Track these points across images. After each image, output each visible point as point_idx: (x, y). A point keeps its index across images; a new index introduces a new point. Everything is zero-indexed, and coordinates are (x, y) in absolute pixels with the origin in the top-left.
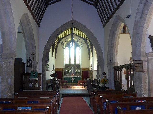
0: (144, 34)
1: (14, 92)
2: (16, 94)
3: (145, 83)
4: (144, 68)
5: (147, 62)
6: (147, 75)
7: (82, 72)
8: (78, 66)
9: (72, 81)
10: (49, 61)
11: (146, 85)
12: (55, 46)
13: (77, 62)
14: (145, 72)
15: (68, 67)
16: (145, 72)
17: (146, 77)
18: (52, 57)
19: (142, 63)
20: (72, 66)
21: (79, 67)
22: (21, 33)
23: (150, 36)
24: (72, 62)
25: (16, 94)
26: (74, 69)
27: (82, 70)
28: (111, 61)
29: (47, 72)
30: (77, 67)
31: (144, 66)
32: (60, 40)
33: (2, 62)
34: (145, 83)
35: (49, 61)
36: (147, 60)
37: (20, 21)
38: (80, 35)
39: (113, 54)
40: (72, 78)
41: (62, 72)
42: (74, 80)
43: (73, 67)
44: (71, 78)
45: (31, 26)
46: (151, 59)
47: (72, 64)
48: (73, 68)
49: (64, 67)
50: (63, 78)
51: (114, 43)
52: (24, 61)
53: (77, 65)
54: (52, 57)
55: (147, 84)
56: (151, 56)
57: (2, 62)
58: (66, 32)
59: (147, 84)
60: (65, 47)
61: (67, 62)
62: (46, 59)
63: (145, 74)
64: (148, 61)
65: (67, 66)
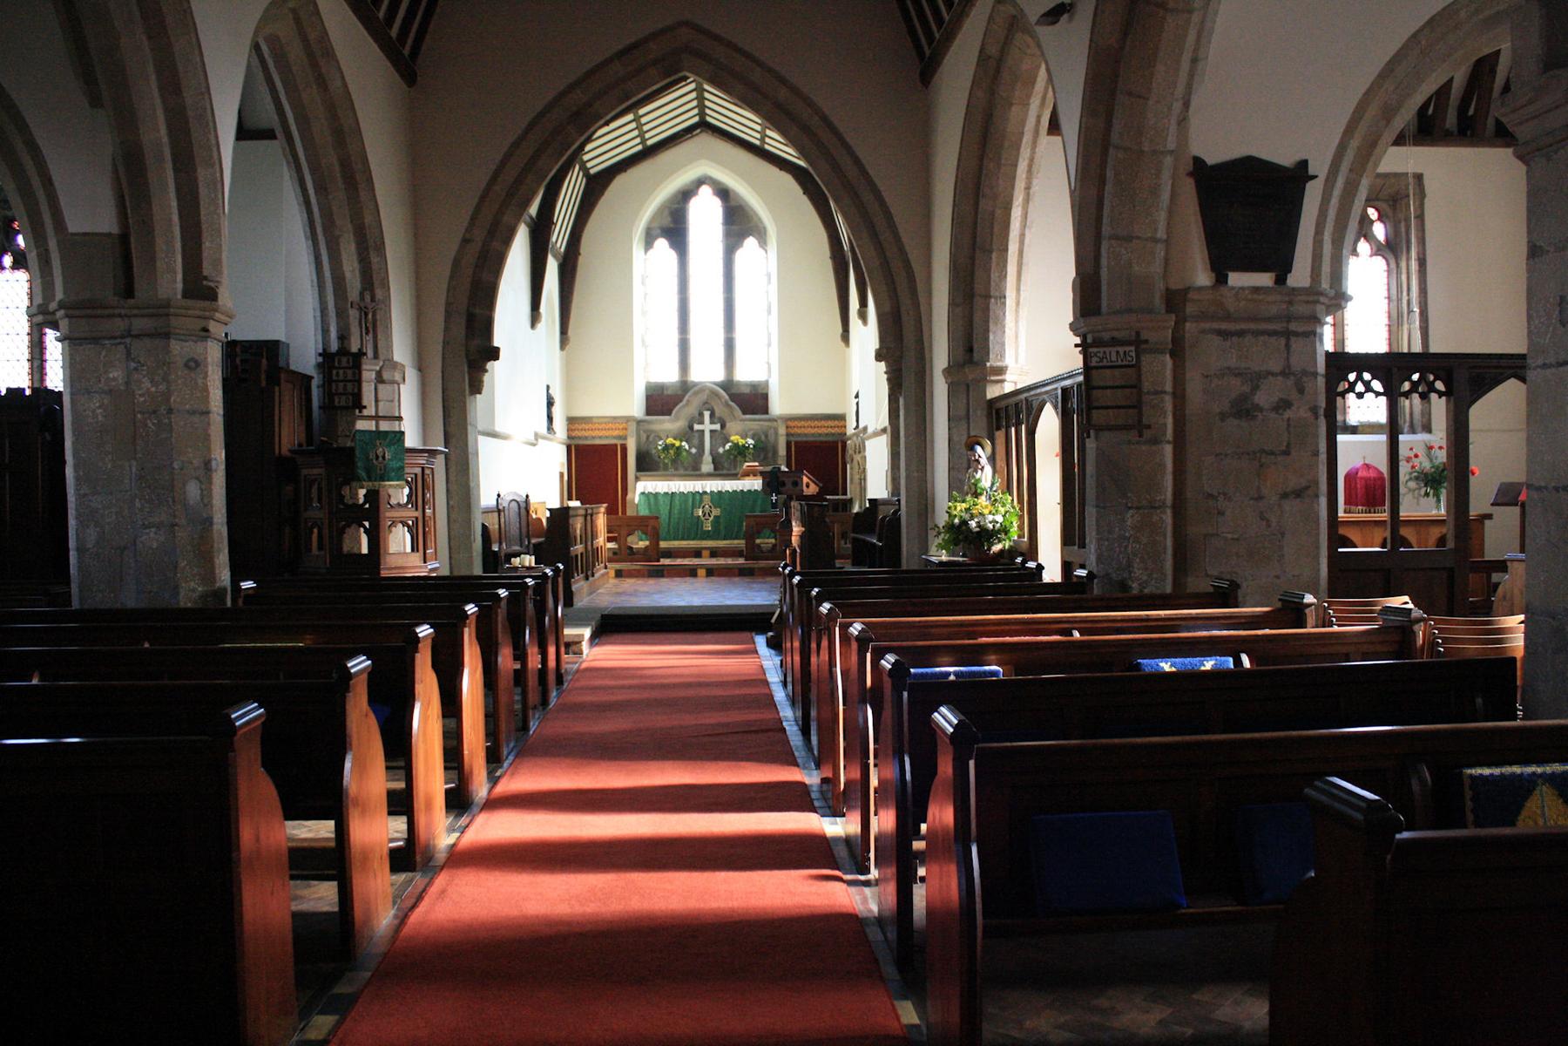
0: (1154, 152)
1: (232, 576)
2: (247, 585)
3: (1154, 507)
4: (1146, 398)
5: (1172, 355)
6: (1168, 450)
7: (788, 444)
8: (753, 400)
9: (708, 527)
10: (494, 354)
11: (1155, 518)
12: (559, 237)
13: (746, 373)
14: (1149, 427)
15: (669, 413)
16: (1149, 427)
17: (1162, 465)
18: (533, 325)
19: (1137, 367)
20: (703, 397)
21: (766, 411)
22: (268, 135)
23: (1198, 162)
24: (707, 370)
25: (247, 585)
26: (717, 427)
27: (782, 431)
28: (976, 356)
29: (482, 440)
30: (744, 413)
31: (1147, 386)
32: (597, 185)
33: (133, 365)
34: (1154, 507)
35: (494, 354)
36: (1174, 340)
37: (256, 47)
38: (762, 140)
39: (988, 297)
40: (707, 499)
41: (624, 449)
42: (716, 512)
43: (706, 405)
44: (949, 674)
45: (339, 83)
46: (1203, 332)
47: (701, 388)
48: (712, 415)
49: (635, 407)
50: (629, 496)
51: (993, 214)
52: (305, 355)
53: (747, 391)
54: (533, 325)
55: (1168, 517)
56: (1202, 316)
57: (133, 365)
58: (643, 120)
59: (1169, 511)
60: (649, 243)
61: (668, 375)
62: (468, 351)
63: (1155, 441)
64: (1177, 350)
65: (660, 401)
